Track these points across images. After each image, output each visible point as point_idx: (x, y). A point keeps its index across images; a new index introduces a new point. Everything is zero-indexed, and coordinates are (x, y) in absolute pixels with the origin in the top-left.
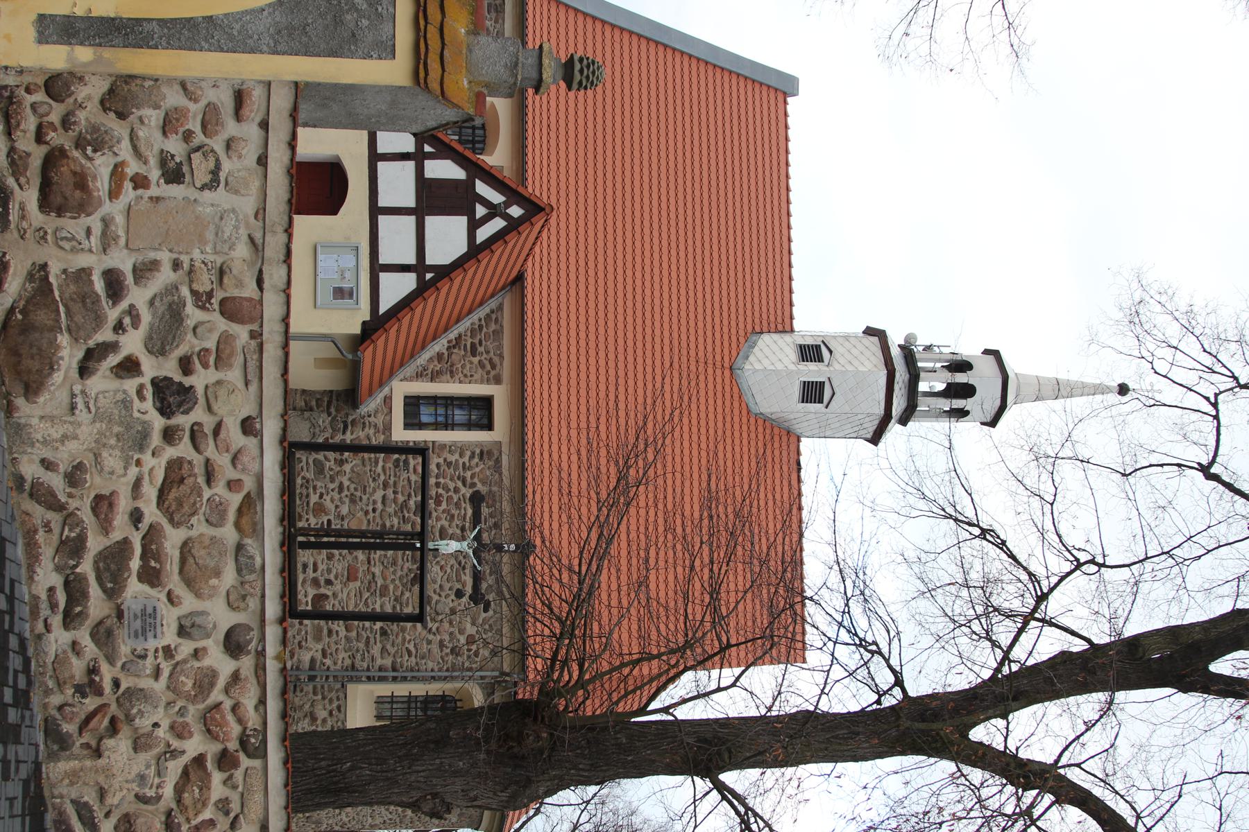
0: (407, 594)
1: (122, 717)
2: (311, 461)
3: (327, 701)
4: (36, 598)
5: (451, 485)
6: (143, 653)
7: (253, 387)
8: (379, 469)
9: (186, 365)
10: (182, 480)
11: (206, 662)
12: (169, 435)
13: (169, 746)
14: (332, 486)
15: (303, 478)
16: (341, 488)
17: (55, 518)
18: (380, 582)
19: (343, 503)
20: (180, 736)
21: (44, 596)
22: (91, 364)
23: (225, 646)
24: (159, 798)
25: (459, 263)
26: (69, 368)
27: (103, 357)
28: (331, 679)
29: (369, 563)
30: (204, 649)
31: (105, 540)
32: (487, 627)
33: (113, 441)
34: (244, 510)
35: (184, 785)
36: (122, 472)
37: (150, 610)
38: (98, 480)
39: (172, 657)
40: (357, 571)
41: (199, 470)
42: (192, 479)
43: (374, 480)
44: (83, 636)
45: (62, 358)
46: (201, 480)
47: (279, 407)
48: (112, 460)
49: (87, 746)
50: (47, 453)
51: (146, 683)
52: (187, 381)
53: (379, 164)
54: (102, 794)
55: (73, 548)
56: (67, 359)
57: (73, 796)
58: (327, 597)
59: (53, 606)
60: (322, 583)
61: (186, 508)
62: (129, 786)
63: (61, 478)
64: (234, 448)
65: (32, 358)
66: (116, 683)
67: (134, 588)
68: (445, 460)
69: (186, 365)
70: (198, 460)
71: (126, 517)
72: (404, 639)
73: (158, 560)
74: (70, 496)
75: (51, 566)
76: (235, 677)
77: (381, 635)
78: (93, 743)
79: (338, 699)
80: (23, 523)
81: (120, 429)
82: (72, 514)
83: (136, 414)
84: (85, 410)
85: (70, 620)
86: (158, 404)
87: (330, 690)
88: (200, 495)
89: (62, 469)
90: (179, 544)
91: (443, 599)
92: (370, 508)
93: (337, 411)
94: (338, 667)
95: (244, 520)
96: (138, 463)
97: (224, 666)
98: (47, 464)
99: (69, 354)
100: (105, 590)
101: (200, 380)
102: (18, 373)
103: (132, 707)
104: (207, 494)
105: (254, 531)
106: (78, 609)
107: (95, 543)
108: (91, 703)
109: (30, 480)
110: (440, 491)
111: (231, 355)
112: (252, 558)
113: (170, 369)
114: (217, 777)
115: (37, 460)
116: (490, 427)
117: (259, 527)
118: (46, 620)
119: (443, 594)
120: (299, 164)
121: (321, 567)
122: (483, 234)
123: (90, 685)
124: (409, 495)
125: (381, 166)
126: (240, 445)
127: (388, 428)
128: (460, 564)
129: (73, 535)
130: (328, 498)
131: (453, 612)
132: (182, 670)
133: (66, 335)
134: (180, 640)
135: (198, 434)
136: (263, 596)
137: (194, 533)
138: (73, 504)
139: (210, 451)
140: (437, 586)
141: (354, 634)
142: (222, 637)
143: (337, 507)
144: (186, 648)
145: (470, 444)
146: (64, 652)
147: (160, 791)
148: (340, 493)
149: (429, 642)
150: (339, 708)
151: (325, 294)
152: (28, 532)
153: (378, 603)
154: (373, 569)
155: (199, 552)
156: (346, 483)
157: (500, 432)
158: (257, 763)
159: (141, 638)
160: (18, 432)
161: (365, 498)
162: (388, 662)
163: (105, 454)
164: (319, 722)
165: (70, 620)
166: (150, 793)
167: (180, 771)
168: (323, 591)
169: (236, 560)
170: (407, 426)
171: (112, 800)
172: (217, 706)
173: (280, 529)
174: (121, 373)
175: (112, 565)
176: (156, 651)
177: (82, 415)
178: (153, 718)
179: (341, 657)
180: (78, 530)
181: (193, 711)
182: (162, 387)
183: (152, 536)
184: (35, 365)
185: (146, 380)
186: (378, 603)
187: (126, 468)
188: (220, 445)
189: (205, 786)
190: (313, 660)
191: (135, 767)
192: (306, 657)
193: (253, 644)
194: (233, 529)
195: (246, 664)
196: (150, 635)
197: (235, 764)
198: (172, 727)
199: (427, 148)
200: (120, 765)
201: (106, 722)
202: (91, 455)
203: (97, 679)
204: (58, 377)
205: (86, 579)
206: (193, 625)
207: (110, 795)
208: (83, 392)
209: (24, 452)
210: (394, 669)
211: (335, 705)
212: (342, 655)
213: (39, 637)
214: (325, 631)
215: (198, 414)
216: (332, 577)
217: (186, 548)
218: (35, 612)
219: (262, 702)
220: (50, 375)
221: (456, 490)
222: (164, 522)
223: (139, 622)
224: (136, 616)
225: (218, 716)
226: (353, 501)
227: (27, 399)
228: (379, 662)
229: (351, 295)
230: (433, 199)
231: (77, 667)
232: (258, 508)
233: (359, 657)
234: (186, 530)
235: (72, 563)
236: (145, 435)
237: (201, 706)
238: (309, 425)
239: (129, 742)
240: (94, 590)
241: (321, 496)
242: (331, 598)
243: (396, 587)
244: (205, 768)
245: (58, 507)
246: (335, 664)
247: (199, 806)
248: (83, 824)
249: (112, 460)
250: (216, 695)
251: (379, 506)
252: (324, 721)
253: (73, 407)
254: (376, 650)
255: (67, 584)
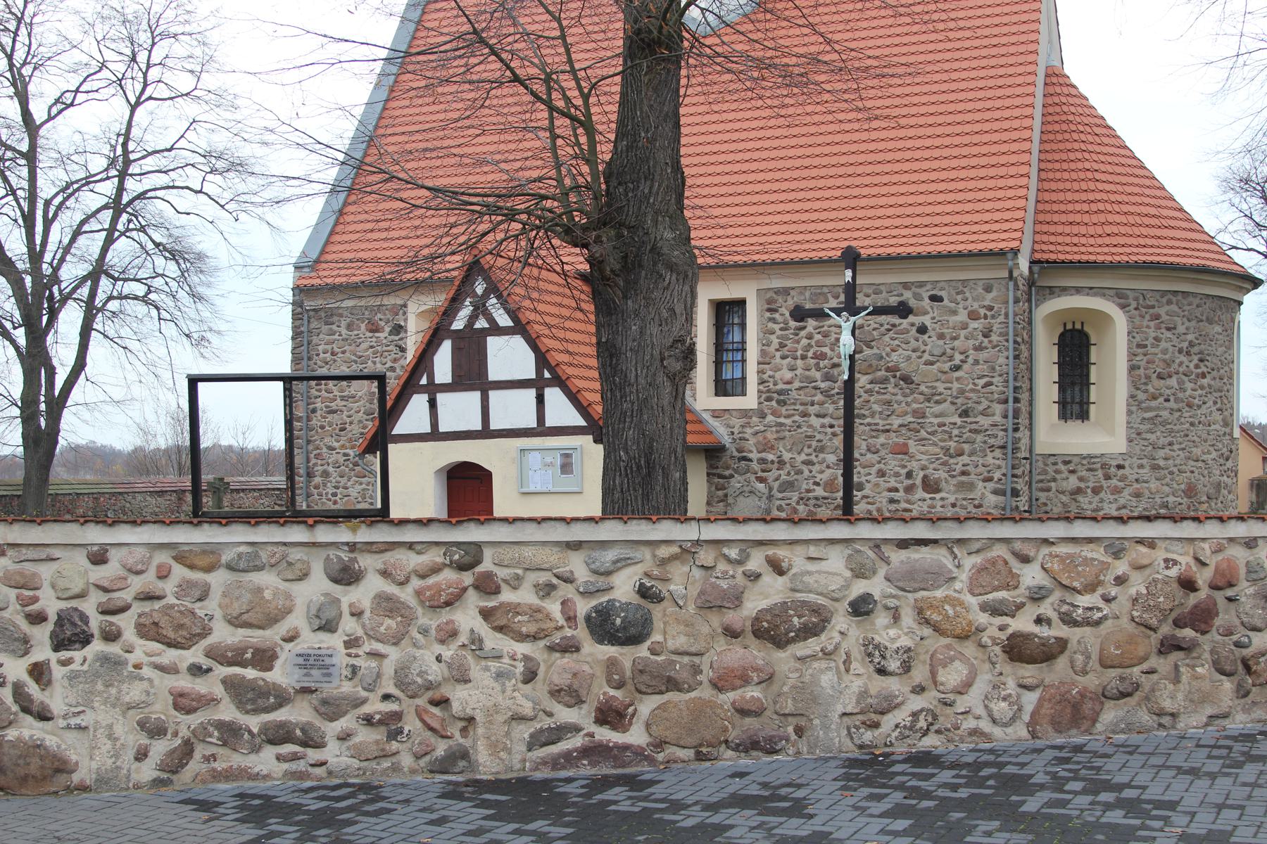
0: (922, 388)
1: (430, 694)
2: (780, 495)
3: (1058, 476)
4: (287, 774)
5: (805, 342)
6: (350, 669)
7: (56, 553)
8: (788, 421)
9: (37, 618)
10: (156, 624)
11: (366, 604)
12: (111, 636)
13: (464, 645)
14: (806, 473)
15: (798, 503)
16: (808, 463)
17: (200, 751)
18: (909, 419)
19: (824, 460)
20: (454, 634)
21: (285, 766)
22: (35, 709)
23: (349, 584)
24: (526, 658)
25: (533, 344)
26: (43, 730)
27: (29, 698)
28: (1016, 472)
29: (888, 431)
30: (350, 606)
31: (224, 702)
32: (959, 297)
33: (113, 691)
34: (188, 562)
35: (514, 632)
36: (146, 684)
37: (301, 661)
38: (158, 707)
39: (357, 639)
40: (897, 444)
41: (147, 607)
42: (155, 615)
43: (799, 427)
44: (332, 729)
45: (31, 737)
46: (157, 605)
47: (74, 527)
48: (134, 692)
49: (464, 731)
50: (130, 754)
51: (389, 667)
52: (53, 618)
53: (441, 430)
54: (518, 718)
55: (230, 734)
56: (34, 732)
57: (524, 749)
58: (925, 477)
59: (295, 757)
60: (910, 482)
61: (186, 621)
62: (509, 689)
63: (154, 742)
64: (123, 573)
65: (28, 764)
66: (386, 697)
67: (281, 675)
68: (777, 350)
69: (37, 618)
70: (137, 608)
71: (198, 680)
72: (972, 390)
73: (244, 650)
74: (176, 734)
75: (253, 757)
76: (385, 574)
77: (968, 416)
78: (461, 724)
79: (1055, 464)
80: (204, 782)
81: (100, 683)
82: (193, 732)
83: (85, 667)
84: (82, 716)
85: (311, 740)
86: (77, 646)
87: (1045, 472)
88: (172, 606)
89: (147, 741)
90: (231, 628)
91: (928, 348)
92: (829, 430)
93: (728, 468)
94: (1002, 463)
95: (199, 562)
96: (138, 667)
97: (373, 585)
98: (141, 755)
99: (28, 729)
100: (280, 706)
101: (51, 605)
102: (44, 778)
103: (415, 682)
104: (171, 600)
105: (212, 552)
106: (298, 732)
107: (228, 712)
108: (411, 724)
109: (158, 773)
110: (810, 354)
111: (21, 574)
112: (240, 555)
113: (41, 635)
114: (507, 596)
115: (137, 764)
116: (742, 303)
117: (206, 548)
118: (312, 765)
119: (923, 348)
120: (451, 513)
121: (893, 483)
122: (504, 320)
123: (391, 724)
124: (816, 388)
125: (443, 428)
126: (118, 565)
127: (745, 413)
128: (889, 330)
129: (216, 733)
130: (819, 476)
131: (941, 336)
132: (372, 629)
133: (8, 731)
134: (340, 630)
135: (111, 607)
136: (285, 544)
137: (218, 614)
138: (184, 732)
139: (126, 596)
140: (914, 355)
141: (966, 446)
142: (339, 588)
143: (828, 467)
144: (349, 625)
145: (760, 323)
146: (348, 748)
147: (519, 656)
148: (814, 464)
149: (976, 362)
150: (1066, 463)
151: (567, 483)
152: (214, 777)
153: (932, 420)
154: (895, 426)
155: (236, 609)
156: (803, 457)
157: (746, 290)
158: (488, 554)
159: (332, 670)
160: (103, 781)
161: (818, 437)
162: (998, 409)
163: (127, 699)
164: (1082, 485)
165: (311, 740)
166: (520, 667)
167: (499, 635)
168: (918, 481)
169: (244, 571)
170: (744, 394)
171: (527, 708)
172: (418, 593)
173: (206, 526)
174: (45, 679)
175: (252, 697)
176: (349, 655)
177: (87, 719)
178: (429, 661)
179: (992, 461)
180: (211, 729)
181: (431, 621)
182: (59, 644)
183: (220, 655)
184: (35, 763)
185: (53, 657)
186: (932, 420)
187: (142, 679)
188: (119, 585)
189: (515, 609)
190: (995, 492)
191: (486, 682)
192: (992, 499)
193: (342, 555)
194: (213, 574)
195: (366, 561)
196: (328, 661)
197: (489, 576)
198: (442, 642)
199: (424, 381)
200: (483, 697)
201: (436, 711)
202: (131, 712)
203: (377, 717)
204: (51, 741)
205: (266, 723)
206: (318, 617)
207: (520, 710)
208: (65, 717)
209: (128, 777)
210: (1006, 401)
211: (1062, 467)
212: (989, 460)
213: (330, 773)
214: (963, 478)
215: (89, 606)
216: (904, 471)
217: (236, 622)
218: (301, 776)
219: (410, 546)
220: (45, 748)
221: (810, 337)
222: (205, 643)
223: (315, 672)
224: (306, 675)
225: (428, 593)
226: (821, 449)
227: (73, 771)
228: (998, 418)
229: (567, 456)
230: (471, 374)
231: (365, 736)
232: (186, 548)
233: (992, 441)
234: (214, 621)
235: (246, 736)
236: (105, 659)
237: (420, 611)
238: (741, 498)
239: (459, 687)
240: (281, 715)
241: (817, 484)
242: (927, 472)
243: (915, 401)
244: (494, 609)
245: (187, 750)
246: (999, 467)
247: (540, 616)
248: (559, 740)
249: (134, 692)
250: (406, 595)
251: (827, 421)
252: (1081, 479)
253: (80, 728)
254: (985, 422)
255: (272, 742)
